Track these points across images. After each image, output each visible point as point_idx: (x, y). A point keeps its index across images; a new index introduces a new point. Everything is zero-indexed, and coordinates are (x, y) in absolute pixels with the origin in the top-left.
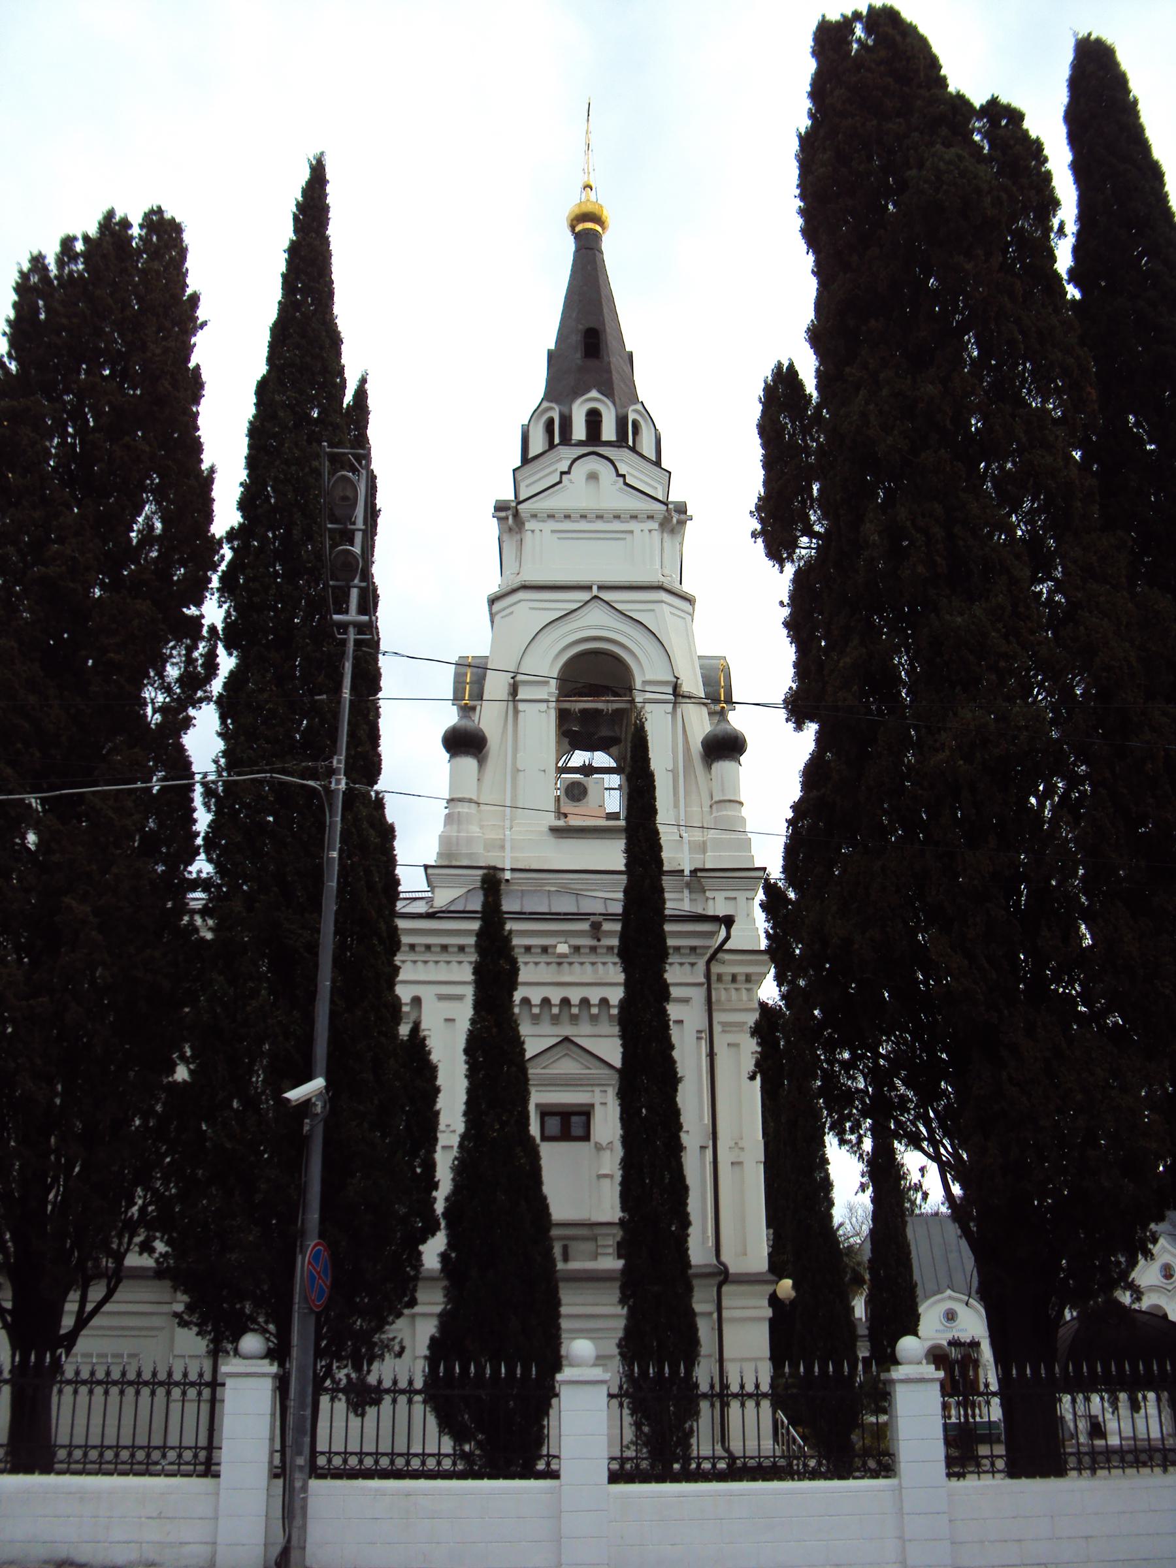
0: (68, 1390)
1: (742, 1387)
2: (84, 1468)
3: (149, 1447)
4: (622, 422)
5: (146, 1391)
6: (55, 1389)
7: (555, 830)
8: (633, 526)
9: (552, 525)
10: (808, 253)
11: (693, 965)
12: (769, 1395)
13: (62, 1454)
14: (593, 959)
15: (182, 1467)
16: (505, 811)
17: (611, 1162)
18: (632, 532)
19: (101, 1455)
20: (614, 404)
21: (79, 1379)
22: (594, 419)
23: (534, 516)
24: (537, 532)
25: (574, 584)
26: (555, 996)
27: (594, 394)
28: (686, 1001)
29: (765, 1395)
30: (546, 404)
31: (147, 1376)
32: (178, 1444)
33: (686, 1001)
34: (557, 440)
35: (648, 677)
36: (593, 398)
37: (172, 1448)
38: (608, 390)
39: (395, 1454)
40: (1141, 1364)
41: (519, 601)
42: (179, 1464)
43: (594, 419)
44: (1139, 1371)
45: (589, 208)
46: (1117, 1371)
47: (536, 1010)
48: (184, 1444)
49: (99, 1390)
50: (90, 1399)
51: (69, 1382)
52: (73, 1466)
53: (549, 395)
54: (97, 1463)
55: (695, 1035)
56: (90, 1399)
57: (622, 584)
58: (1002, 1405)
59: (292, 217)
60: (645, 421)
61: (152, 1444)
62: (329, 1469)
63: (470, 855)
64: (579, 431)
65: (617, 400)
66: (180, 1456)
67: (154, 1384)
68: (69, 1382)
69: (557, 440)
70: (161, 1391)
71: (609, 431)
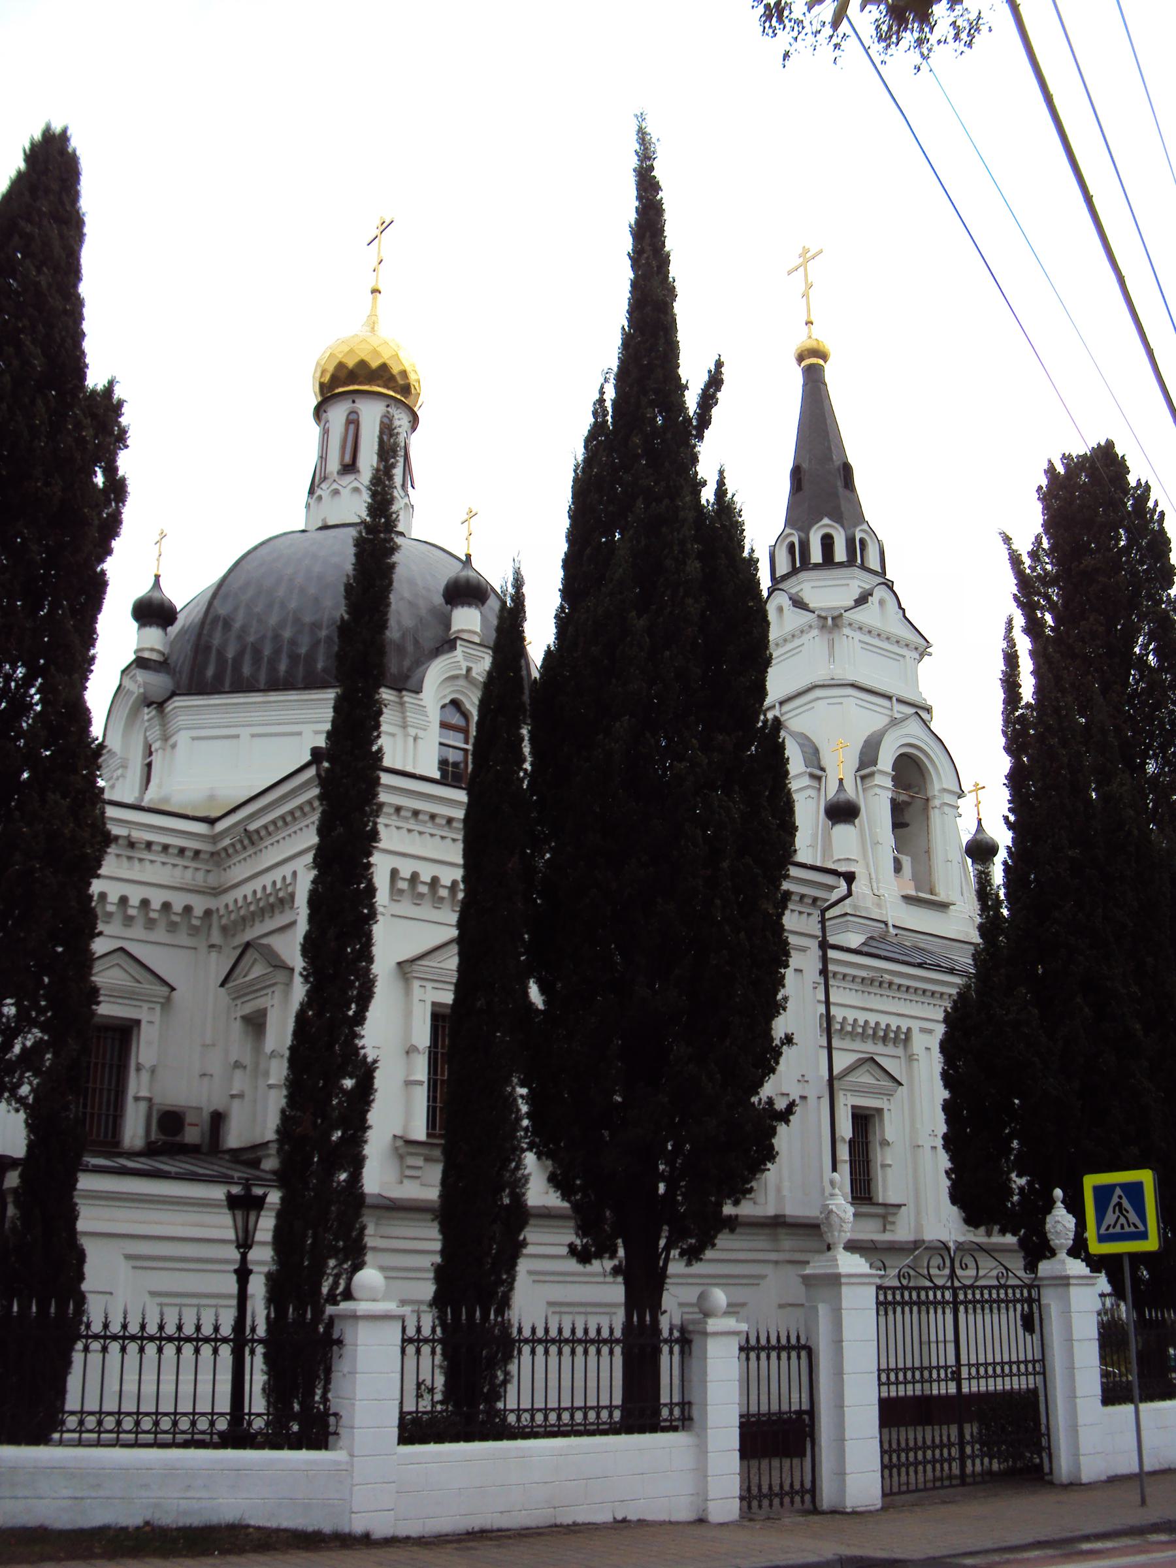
0: (96, 1345)
1: (143, 1327)
2: (80, 1438)
3: (119, 1413)
4: (850, 543)
5: (170, 1349)
6: (79, 1346)
7: (907, 899)
8: (805, 638)
9: (858, 636)
10: (715, 381)
11: (809, 914)
12: (231, 1340)
13: (72, 1422)
14: (178, 861)
15: (85, 1435)
16: (823, 860)
17: (137, 1085)
18: (904, 657)
19: (156, 1423)
20: (843, 526)
21: (90, 1333)
22: (827, 542)
23: (850, 625)
24: (850, 638)
25: (912, 702)
26: (135, 895)
27: (826, 521)
28: (803, 949)
29: (225, 1340)
30: (788, 531)
31: (115, 1328)
32: (530, 1407)
33: (803, 949)
34: (798, 565)
35: (945, 786)
36: (825, 525)
37: (72, 1413)
38: (838, 517)
39: (142, 1413)
40: (464, 1310)
41: (848, 696)
42: (99, 1432)
43: (827, 542)
44: (645, 1321)
45: (811, 344)
46: (651, 1321)
47: (195, 922)
48: (87, 1408)
49: (188, 1349)
50: (758, 1364)
51: (96, 1337)
52: (601, 1427)
53: (790, 521)
54: (95, 1432)
55: (812, 985)
56: (758, 1364)
57: (907, 700)
58: (623, 1353)
59: (1001, 656)
60: (871, 538)
61: (521, 1407)
62: (532, 1427)
63: (867, 909)
64: (816, 556)
65: (845, 525)
66: (81, 1423)
67: (161, 1339)
68: (96, 1337)
69: (798, 565)
70: (151, 1348)
71: (840, 554)
